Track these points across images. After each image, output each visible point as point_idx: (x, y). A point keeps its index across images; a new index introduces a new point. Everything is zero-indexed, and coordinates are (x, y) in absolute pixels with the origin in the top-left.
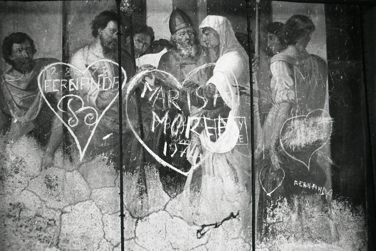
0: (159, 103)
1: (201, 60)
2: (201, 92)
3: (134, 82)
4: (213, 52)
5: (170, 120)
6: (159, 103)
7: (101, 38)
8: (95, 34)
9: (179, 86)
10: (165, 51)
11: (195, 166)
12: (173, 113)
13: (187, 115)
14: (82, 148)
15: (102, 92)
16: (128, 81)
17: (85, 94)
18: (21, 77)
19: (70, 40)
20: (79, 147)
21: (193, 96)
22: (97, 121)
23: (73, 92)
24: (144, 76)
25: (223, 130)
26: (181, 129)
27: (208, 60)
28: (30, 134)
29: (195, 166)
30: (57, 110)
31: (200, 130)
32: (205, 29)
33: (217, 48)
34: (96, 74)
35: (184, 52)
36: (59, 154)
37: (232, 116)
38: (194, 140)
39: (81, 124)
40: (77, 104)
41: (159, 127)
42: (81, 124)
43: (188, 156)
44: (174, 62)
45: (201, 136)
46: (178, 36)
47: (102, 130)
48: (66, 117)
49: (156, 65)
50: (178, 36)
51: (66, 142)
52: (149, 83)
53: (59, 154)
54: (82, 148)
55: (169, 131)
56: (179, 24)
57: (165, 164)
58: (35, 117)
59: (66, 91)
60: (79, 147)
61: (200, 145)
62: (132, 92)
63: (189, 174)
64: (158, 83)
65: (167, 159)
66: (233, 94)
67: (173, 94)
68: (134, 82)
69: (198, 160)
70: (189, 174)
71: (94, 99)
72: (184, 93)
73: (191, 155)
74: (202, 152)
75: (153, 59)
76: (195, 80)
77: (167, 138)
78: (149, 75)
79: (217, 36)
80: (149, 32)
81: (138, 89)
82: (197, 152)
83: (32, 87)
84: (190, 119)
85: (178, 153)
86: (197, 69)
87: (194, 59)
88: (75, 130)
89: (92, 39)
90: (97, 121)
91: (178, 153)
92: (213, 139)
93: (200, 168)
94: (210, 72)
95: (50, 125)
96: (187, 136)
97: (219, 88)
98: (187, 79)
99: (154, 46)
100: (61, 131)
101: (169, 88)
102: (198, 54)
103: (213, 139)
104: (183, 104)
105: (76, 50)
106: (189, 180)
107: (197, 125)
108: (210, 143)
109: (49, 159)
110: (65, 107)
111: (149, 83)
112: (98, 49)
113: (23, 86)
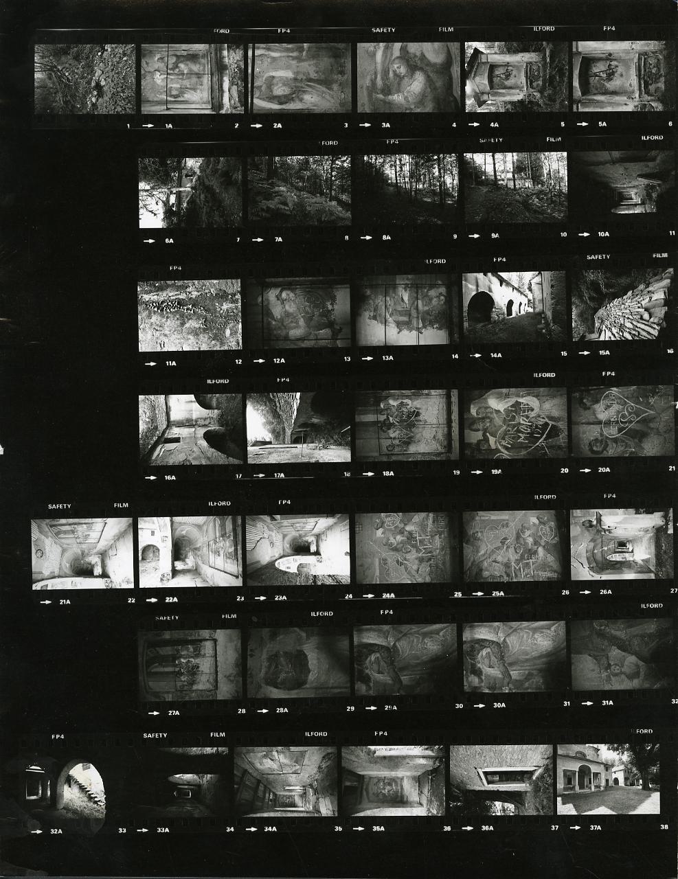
0: (513, 438)
1: (492, 416)
2: (508, 416)
3: (503, 450)
4: (488, 410)
5: (523, 433)
6: (513, 438)
7: (591, 405)
8: (589, 408)
9: (505, 428)
10: (488, 434)
11: (547, 420)
12: (519, 431)
13: (520, 424)
14: (647, 412)
15: (617, 403)
16: (502, 452)
17: (618, 412)
18: (610, 446)
19: (591, 421)
20: (647, 414)
21: (510, 421)
22: (632, 404)
23: (618, 418)
24: (500, 445)
25: (527, 404)
26: (527, 427)
27: (491, 413)
28: (640, 441)
29: (547, 420)
30: (627, 427)
31: (527, 417)
32: (477, 414)
33: (487, 408)
34: (608, 407)
35: (488, 425)
36: (652, 425)
37: (521, 400)
38: (533, 420)
39: (634, 413)
40: (624, 416)
41: (526, 438)
42: (634, 413)
43: (541, 423)
44: (494, 429)
45: (531, 416)
46: (481, 428)
47: (638, 403)
48: (631, 422)
49: (495, 439)
50: (481, 428)
51: (645, 421)
52: (503, 443)
53: (652, 425)
54: (647, 412)
55: (528, 433)
56: (475, 427)
57: (544, 436)
58: (631, 439)
59: (617, 422)
60: (647, 414)
61: (536, 418)
62: (508, 451)
63: (551, 423)
64: (503, 438)
65: (542, 435)
66: (509, 399)
67: (509, 431)
68: (503, 450)
69: (543, 418)
70: (551, 423)
71: (621, 407)
72: (508, 425)
73: (541, 422)
74: (539, 416)
75: (492, 440)
76: (502, 419)
77: (531, 434)
78: (500, 443)
79: (480, 408)
80: (479, 441)
81: (507, 448)
82: (540, 419)
83: (615, 440)
84: (522, 422)
85: (539, 428)
86: (497, 419)
87: (491, 420)
88: (638, 417)
89: (591, 411)
90: (632, 404)
91: (539, 428)
92: (532, 410)
93: (548, 417)
94: (498, 412)
95: (637, 431)
96: (530, 424)
97: (506, 407)
98: (501, 423)
99: (486, 440)
100: (638, 425)
101: (506, 433)
102: (489, 418)
103: (532, 410)
104: (514, 426)
105: (596, 418)
106: (553, 423)
107: (525, 419)
108: (535, 412)
109: (655, 430)
110: (626, 422)
111: (503, 443)
112: (596, 406)
113: (615, 445)
